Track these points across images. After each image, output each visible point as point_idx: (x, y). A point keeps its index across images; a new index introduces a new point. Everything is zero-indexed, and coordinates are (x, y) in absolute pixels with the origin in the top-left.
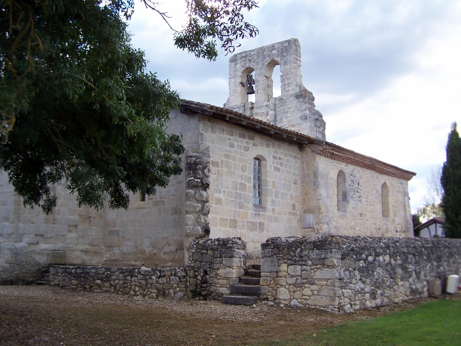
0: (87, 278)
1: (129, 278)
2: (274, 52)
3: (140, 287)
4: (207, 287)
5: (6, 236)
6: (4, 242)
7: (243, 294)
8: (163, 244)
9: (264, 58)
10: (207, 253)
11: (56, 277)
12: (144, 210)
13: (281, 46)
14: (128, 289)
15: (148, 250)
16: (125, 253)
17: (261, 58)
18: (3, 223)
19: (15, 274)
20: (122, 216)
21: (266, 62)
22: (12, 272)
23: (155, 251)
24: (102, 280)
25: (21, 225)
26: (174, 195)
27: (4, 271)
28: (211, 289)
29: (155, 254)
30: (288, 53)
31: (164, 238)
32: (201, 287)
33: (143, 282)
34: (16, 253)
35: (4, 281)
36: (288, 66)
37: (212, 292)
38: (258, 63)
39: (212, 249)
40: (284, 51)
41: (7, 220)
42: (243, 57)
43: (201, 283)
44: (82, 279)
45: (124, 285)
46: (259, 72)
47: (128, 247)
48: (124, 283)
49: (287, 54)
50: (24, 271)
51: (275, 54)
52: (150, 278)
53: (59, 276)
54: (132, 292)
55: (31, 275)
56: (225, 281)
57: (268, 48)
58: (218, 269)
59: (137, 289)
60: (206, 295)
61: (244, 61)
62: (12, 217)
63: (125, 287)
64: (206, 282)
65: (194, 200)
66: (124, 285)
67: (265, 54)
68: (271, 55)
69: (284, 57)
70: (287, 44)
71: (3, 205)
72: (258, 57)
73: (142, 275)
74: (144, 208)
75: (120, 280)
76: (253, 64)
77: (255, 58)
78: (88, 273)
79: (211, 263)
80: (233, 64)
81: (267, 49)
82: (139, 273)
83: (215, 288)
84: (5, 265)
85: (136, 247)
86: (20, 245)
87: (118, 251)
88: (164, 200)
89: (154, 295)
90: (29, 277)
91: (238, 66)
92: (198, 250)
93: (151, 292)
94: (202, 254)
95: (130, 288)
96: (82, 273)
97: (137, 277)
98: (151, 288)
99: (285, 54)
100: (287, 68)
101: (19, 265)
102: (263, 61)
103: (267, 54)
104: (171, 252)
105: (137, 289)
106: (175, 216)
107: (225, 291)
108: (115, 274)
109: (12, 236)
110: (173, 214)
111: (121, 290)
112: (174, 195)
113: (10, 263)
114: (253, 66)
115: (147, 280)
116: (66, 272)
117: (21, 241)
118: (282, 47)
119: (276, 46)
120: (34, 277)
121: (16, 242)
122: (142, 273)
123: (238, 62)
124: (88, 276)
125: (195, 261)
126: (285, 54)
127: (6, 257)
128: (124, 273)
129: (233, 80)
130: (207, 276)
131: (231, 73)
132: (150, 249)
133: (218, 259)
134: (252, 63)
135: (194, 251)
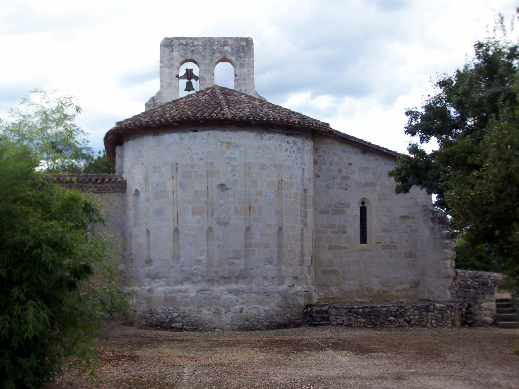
0: (378, 316)
1: (425, 313)
2: (226, 48)
3: (436, 320)
4: (472, 316)
5: (271, 279)
6: (269, 285)
7: (505, 320)
8: (395, 283)
9: (214, 53)
10: (469, 291)
11: (339, 317)
12: (370, 253)
13: (236, 44)
14: (425, 323)
15: (376, 288)
16: (346, 292)
17: (208, 52)
18: (266, 266)
19: (287, 317)
20: (341, 256)
21: (217, 58)
22: (284, 315)
23: (385, 289)
24: (395, 316)
25: (284, 268)
26: (407, 241)
27: (277, 315)
28: (477, 318)
29: (385, 292)
30: (246, 54)
31: (396, 278)
32: (466, 317)
33: (440, 316)
34: (285, 296)
35: (278, 325)
36: (246, 70)
37: (477, 320)
38: (204, 57)
39: (474, 288)
40: (241, 50)
41: (270, 263)
42: (182, 44)
43: (466, 314)
44: (372, 317)
45: (421, 320)
46: (207, 69)
47: (351, 285)
48: (420, 318)
49: (244, 55)
50: (293, 313)
51: (228, 52)
52: (446, 313)
53: (342, 316)
54: (429, 325)
55: (298, 317)
56: (489, 312)
57: (219, 41)
58: (482, 303)
59: (434, 321)
60: (472, 323)
61: (185, 50)
62: (275, 261)
63: (421, 321)
64: (471, 313)
65: (450, 249)
66: (421, 320)
67: (215, 48)
68: (223, 51)
69: (241, 57)
70: (244, 44)
71: (266, 247)
72: (205, 49)
73: (437, 310)
74: (369, 251)
75: (415, 316)
76: (197, 56)
77: (200, 50)
78: (379, 312)
79: (475, 298)
80: (167, 50)
81: (216, 43)
82: (435, 308)
83: (480, 317)
84: (277, 308)
85: (361, 286)
86: (284, 287)
87: (337, 290)
88: (396, 244)
89: (451, 325)
90: (297, 319)
91: (175, 54)
92: (462, 289)
93: (448, 323)
94: (466, 291)
95: (427, 322)
96: (370, 312)
97: (433, 312)
98: (447, 320)
99: (242, 55)
100: (244, 72)
101: (289, 308)
102: (212, 56)
103: (218, 49)
104: (404, 290)
105: (434, 321)
106: (409, 259)
107: (489, 319)
108: (410, 311)
109: (276, 279)
110: (407, 258)
111: (417, 323)
112: (407, 241)
113: (282, 307)
114: (198, 59)
115: (442, 314)
116: (350, 312)
117: (283, 283)
118: (238, 46)
119: (230, 42)
120: (301, 318)
121: (279, 285)
122: (438, 308)
123: (176, 49)
124: (379, 314)
125: (459, 297)
126: (242, 55)
127: (276, 300)
128: (419, 310)
129: (167, 70)
130: (472, 309)
131: (165, 60)
132: (379, 287)
133: (481, 296)
134: (196, 56)
135: (457, 289)
